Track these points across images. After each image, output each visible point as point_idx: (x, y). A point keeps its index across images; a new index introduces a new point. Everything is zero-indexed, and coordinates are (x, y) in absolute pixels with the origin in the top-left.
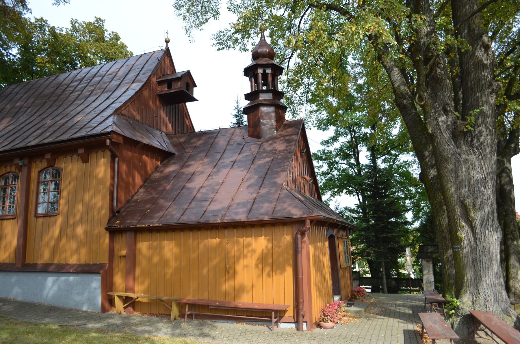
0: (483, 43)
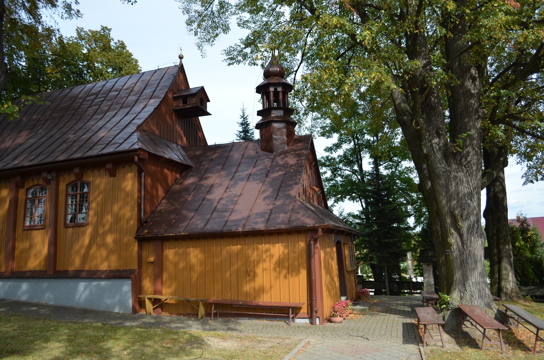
0: (471, 75)
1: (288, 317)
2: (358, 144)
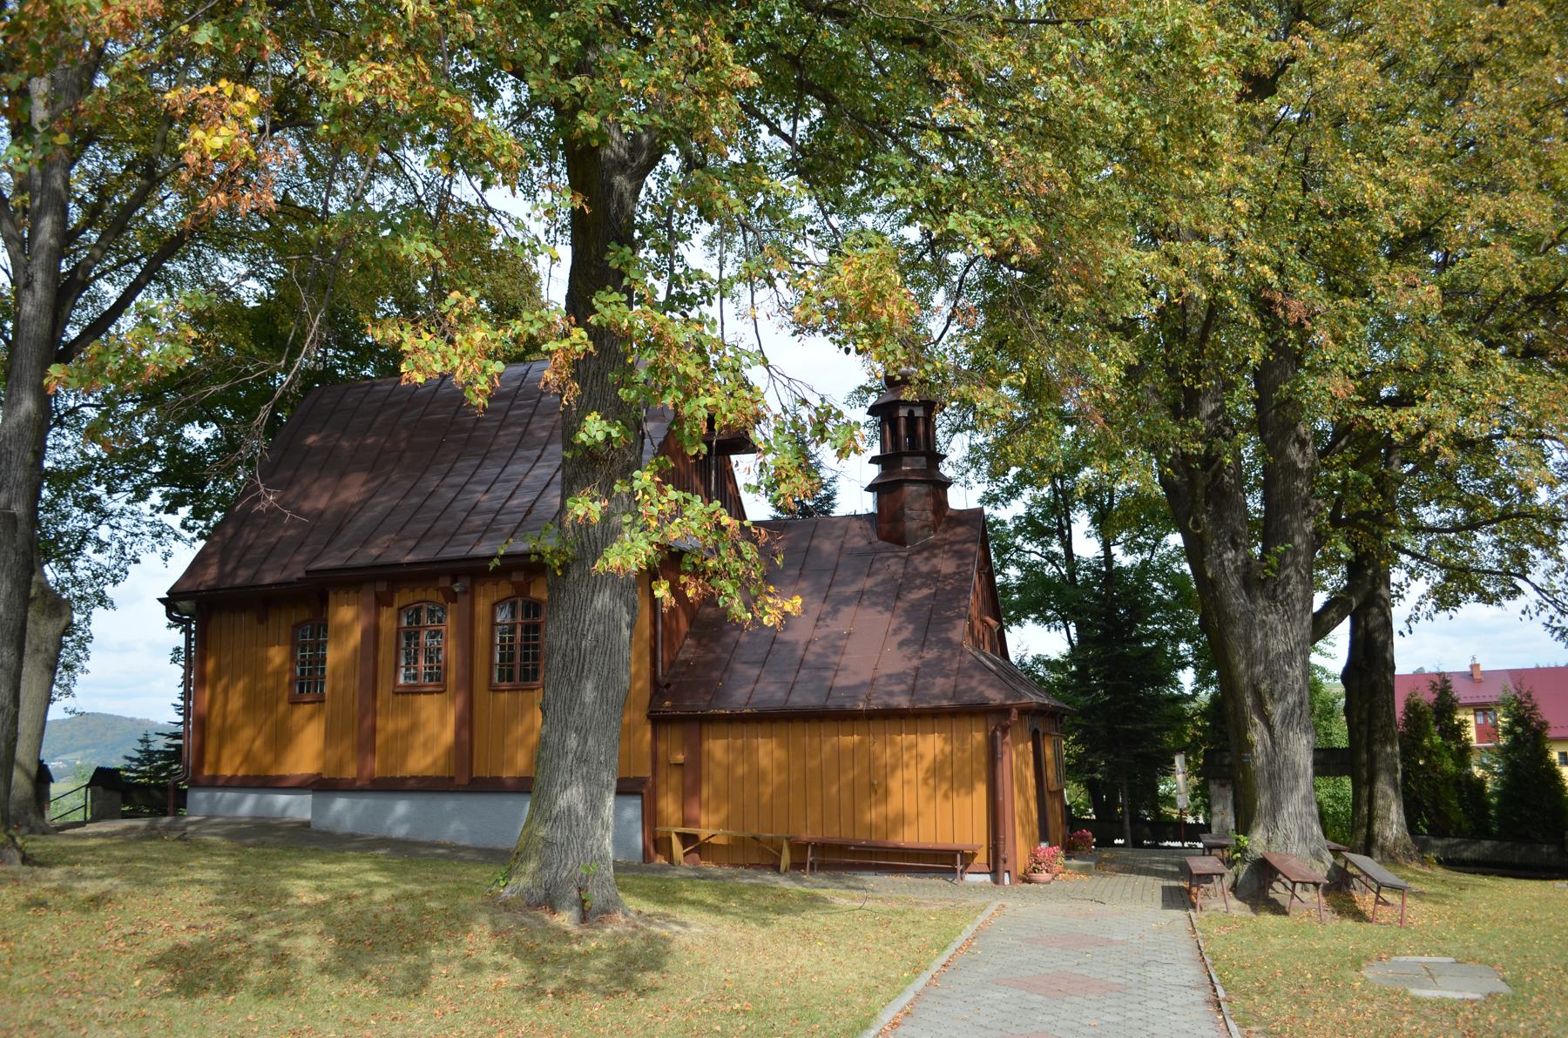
1: (955, 871)
2: (1062, 491)
